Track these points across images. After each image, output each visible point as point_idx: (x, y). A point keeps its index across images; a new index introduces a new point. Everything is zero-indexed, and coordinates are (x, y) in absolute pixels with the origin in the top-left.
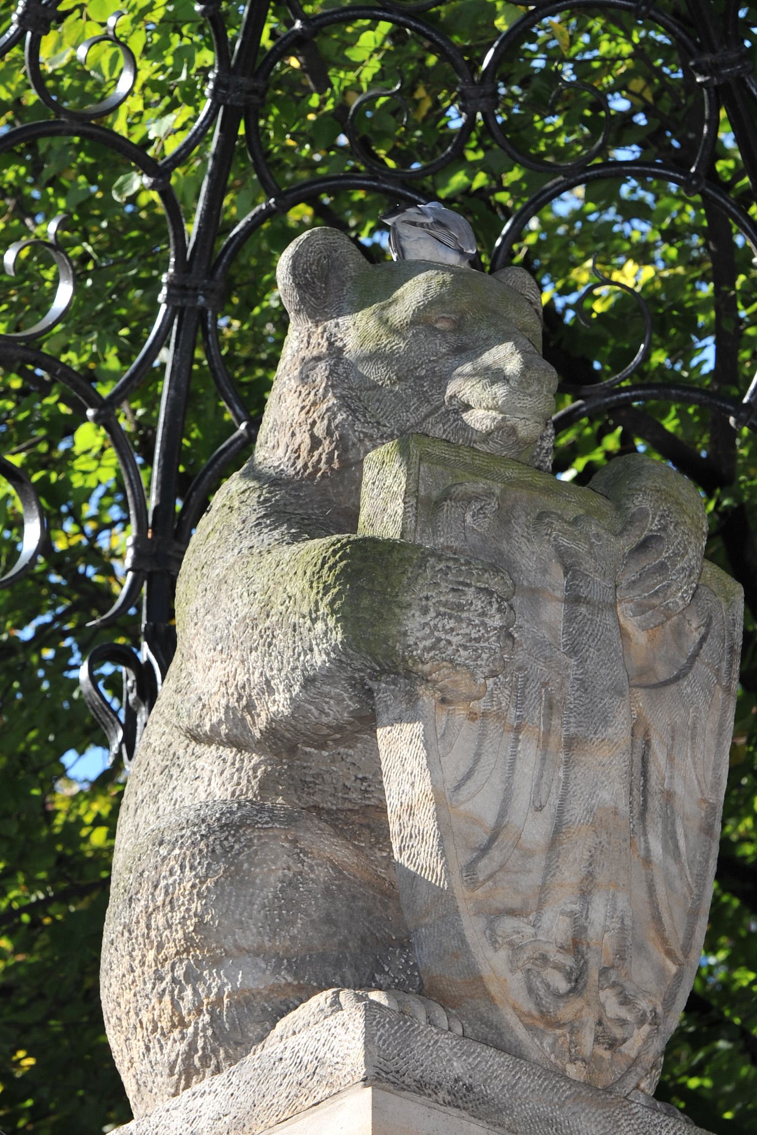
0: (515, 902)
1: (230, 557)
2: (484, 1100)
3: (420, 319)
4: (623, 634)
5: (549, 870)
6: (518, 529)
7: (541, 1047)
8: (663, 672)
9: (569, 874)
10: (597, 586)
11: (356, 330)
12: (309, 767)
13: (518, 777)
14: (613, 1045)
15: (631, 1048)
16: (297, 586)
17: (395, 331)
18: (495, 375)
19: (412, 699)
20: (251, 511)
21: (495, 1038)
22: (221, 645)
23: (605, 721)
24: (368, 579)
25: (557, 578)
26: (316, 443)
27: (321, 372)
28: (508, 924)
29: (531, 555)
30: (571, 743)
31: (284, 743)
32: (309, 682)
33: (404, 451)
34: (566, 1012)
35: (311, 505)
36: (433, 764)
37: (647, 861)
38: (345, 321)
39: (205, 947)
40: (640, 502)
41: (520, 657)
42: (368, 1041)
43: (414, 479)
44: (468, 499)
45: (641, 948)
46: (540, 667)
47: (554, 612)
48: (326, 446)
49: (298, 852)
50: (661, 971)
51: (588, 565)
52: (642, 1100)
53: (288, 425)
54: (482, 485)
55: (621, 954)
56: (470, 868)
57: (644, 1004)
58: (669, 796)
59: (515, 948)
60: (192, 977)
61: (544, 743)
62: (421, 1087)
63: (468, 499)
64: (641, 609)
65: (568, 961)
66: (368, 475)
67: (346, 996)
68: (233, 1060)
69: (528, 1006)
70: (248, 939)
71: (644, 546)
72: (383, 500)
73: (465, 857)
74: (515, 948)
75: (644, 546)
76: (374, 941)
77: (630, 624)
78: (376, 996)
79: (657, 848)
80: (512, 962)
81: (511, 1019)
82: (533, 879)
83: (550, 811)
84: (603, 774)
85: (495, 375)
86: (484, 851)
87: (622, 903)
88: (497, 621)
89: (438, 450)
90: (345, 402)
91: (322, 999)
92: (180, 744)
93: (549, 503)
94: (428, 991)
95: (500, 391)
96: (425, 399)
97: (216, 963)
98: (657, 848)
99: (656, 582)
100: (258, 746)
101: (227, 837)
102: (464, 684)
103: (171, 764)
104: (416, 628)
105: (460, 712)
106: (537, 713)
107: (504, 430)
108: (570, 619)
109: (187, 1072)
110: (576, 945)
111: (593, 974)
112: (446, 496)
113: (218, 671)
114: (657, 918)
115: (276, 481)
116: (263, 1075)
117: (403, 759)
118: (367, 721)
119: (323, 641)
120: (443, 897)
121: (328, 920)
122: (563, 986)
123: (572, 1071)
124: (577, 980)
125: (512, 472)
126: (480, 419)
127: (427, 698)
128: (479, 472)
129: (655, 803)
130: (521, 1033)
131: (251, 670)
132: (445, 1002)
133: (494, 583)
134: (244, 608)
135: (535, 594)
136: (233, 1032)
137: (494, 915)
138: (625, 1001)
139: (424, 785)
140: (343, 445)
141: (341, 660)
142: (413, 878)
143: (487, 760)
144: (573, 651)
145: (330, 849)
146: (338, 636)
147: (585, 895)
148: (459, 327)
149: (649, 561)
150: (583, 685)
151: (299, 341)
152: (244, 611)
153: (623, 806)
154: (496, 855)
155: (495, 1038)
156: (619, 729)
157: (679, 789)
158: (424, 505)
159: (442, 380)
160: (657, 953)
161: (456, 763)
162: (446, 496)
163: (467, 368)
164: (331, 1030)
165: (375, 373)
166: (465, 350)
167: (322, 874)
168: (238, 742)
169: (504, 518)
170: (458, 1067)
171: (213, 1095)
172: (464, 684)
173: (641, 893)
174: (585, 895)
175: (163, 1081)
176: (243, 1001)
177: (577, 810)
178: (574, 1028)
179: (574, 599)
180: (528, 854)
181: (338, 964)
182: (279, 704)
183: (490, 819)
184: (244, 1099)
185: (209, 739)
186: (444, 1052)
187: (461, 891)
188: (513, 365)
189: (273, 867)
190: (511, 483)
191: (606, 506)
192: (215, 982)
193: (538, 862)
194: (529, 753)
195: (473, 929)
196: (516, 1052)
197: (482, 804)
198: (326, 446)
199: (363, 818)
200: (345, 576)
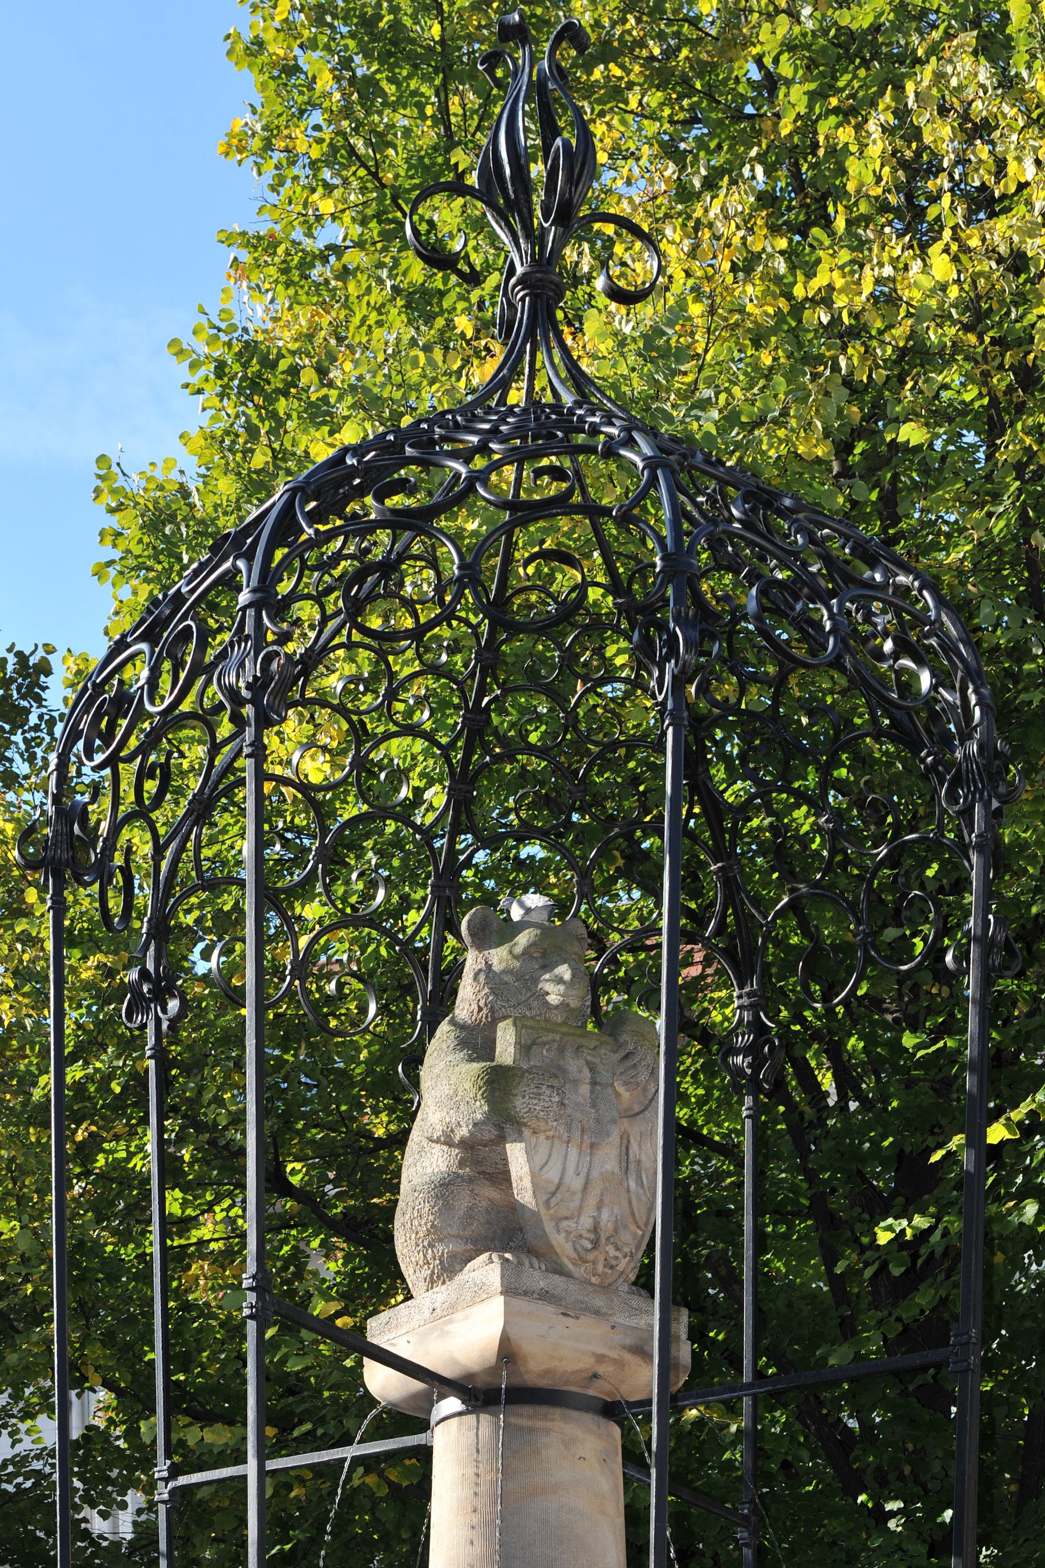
0: (568, 1214)
1: (442, 1065)
2: (554, 1296)
3: (526, 952)
4: (618, 1095)
5: (582, 1200)
6: (568, 1055)
7: (579, 1272)
8: (637, 1108)
9: (592, 1201)
10: (604, 1076)
11: (499, 957)
12: (480, 1157)
13: (568, 1163)
14: (612, 1267)
15: (621, 1267)
16: (468, 1085)
17: (516, 957)
18: (560, 980)
19: (520, 1133)
20: (452, 1042)
21: (559, 1270)
22: (439, 1104)
23: (608, 1135)
24: (498, 1084)
25: (587, 1074)
26: (480, 1009)
27: (482, 977)
28: (565, 1224)
29: (575, 1066)
30: (592, 1146)
31: (467, 1146)
32: (475, 1125)
33: (515, 1024)
34: (591, 1257)
35: (477, 1042)
36: (530, 1160)
37: (628, 1191)
38: (493, 951)
39: (436, 1234)
40: (625, 1037)
41: (569, 1111)
42: (502, 1277)
43: (518, 1035)
44: (544, 1044)
45: (625, 1227)
46: (578, 1115)
47: (585, 1089)
48: (485, 1011)
49: (473, 1194)
50: (635, 1235)
51: (600, 1067)
52: (625, 1288)
53: (469, 999)
54: (550, 1037)
55: (616, 1230)
56: (547, 1203)
57: (626, 1250)
58: (639, 1162)
59: (568, 1233)
60: (431, 1245)
61: (580, 1147)
62: (526, 1293)
63: (544, 1044)
64: (625, 1084)
65: (592, 1236)
66: (499, 1034)
67: (495, 1256)
68: (451, 1279)
69: (574, 1256)
70: (454, 1231)
71: (626, 1057)
72: (506, 1044)
73: (545, 1197)
74: (568, 1233)
75: (626, 1057)
76: (508, 1233)
77: (621, 1090)
78: (507, 1255)
79: (632, 1184)
80: (567, 1240)
81: (566, 1261)
82: (577, 1203)
83: (583, 1175)
84: (608, 1160)
85: (560, 980)
86: (554, 1194)
87: (616, 1210)
88: (557, 1099)
89: (530, 1023)
90: (493, 991)
91: (485, 1256)
92: (425, 1142)
93: (583, 1041)
94: (532, 1252)
95: (562, 988)
96: (529, 989)
97: (441, 1240)
98: (632, 1184)
99: (633, 1073)
100: (457, 1146)
101: (444, 1189)
102: (542, 1125)
103: (422, 1150)
104: (520, 1104)
105: (542, 1137)
106: (577, 1135)
107: (564, 1006)
108: (592, 1092)
109: (432, 1282)
110: (595, 1229)
111: (603, 1240)
112: (534, 1043)
113: (438, 1115)
114: (633, 1214)
115: (461, 1027)
116: (461, 1287)
117: (516, 1154)
118: (502, 1139)
119: (480, 1109)
120: (536, 1215)
121: (488, 1222)
122: (589, 1246)
123: (594, 1280)
124: (596, 1244)
125: (564, 1029)
126: (553, 999)
127: (527, 1132)
128: (549, 1031)
129: (632, 1166)
130: (571, 1267)
131: (453, 1117)
132: (538, 1256)
133: (555, 1083)
134: (447, 1091)
135: (576, 1082)
136: (449, 1268)
137: (558, 1220)
138: (617, 1249)
139: (526, 1169)
140: (492, 1010)
141: (488, 1117)
142: (523, 1206)
143: (554, 1156)
144: (593, 1106)
145: (489, 1192)
146: (486, 1108)
147: (599, 1208)
148: (544, 955)
149: (630, 1063)
150: (598, 1121)
151: (472, 961)
152: (447, 1090)
153: (616, 1170)
154: (559, 1196)
155: (559, 1270)
156: (615, 1138)
157: (643, 1158)
158: (524, 1048)
159: (536, 981)
160: (633, 1228)
161: (540, 1158)
162: (534, 1043)
163: (547, 976)
164: (486, 1271)
165: (506, 978)
166: (547, 967)
167: (484, 1203)
168: (449, 1143)
169: (561, 1050)
170: (542, 1284)
171: (442, 1294)
172: (542, 1125)
173: (626, 1204)
174: (599, 1208)
175: (423, 1285)
176: (453, 1256)
177: (595, 1174)
178: (594, 1263)
179: (594, 1083)
180: (574, 1194)
181: (492, 1240)
182: (463, 1132)
183: (556, 1181)
184: (454, 1296)
185: (437, 1141)
186: (537, 1278)
187: (543, 1212)
188: (567, 976)
189: (463, 1202)
190: (564, 1034)
191: (610, 1040)
192: (440, 1248)
193: (579, 1196)
194: (573, 1152)
195: (549, 1227)
196: (568, 1275)
197: (552, 1174)
198: (485, 1011)
199: (501, 1177)
200: (488, 1083)
